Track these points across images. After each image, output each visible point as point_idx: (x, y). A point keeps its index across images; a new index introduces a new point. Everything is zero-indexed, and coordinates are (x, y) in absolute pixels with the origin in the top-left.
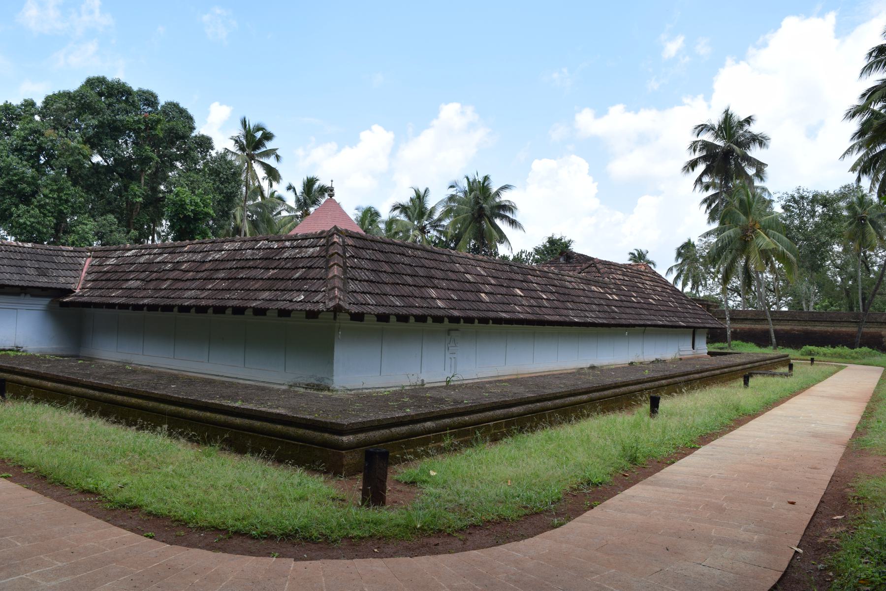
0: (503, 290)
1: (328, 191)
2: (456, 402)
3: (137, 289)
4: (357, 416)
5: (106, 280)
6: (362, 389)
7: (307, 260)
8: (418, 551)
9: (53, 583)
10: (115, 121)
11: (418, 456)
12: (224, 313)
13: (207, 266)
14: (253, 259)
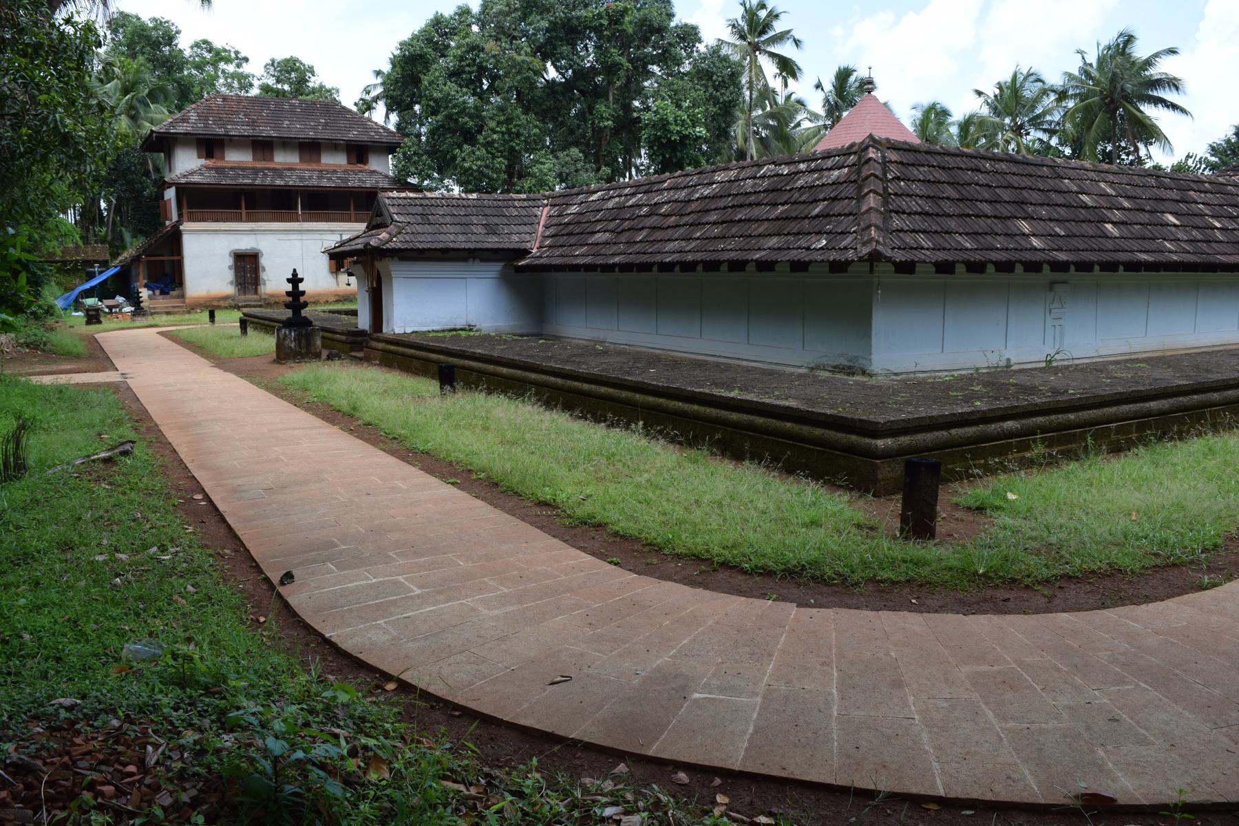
0: (1145, 217)
1: (867, 85)
2: (1055, 391)
3: (606, 243)
4: (900, 410)
5: (567, 234)
7: (830, 188)
8: (976, 606)
9: (497, 612)
10: (570, 20)
11: (989, 470)
12: (718, 270)
13: (693, 206)
14: (755, 192)
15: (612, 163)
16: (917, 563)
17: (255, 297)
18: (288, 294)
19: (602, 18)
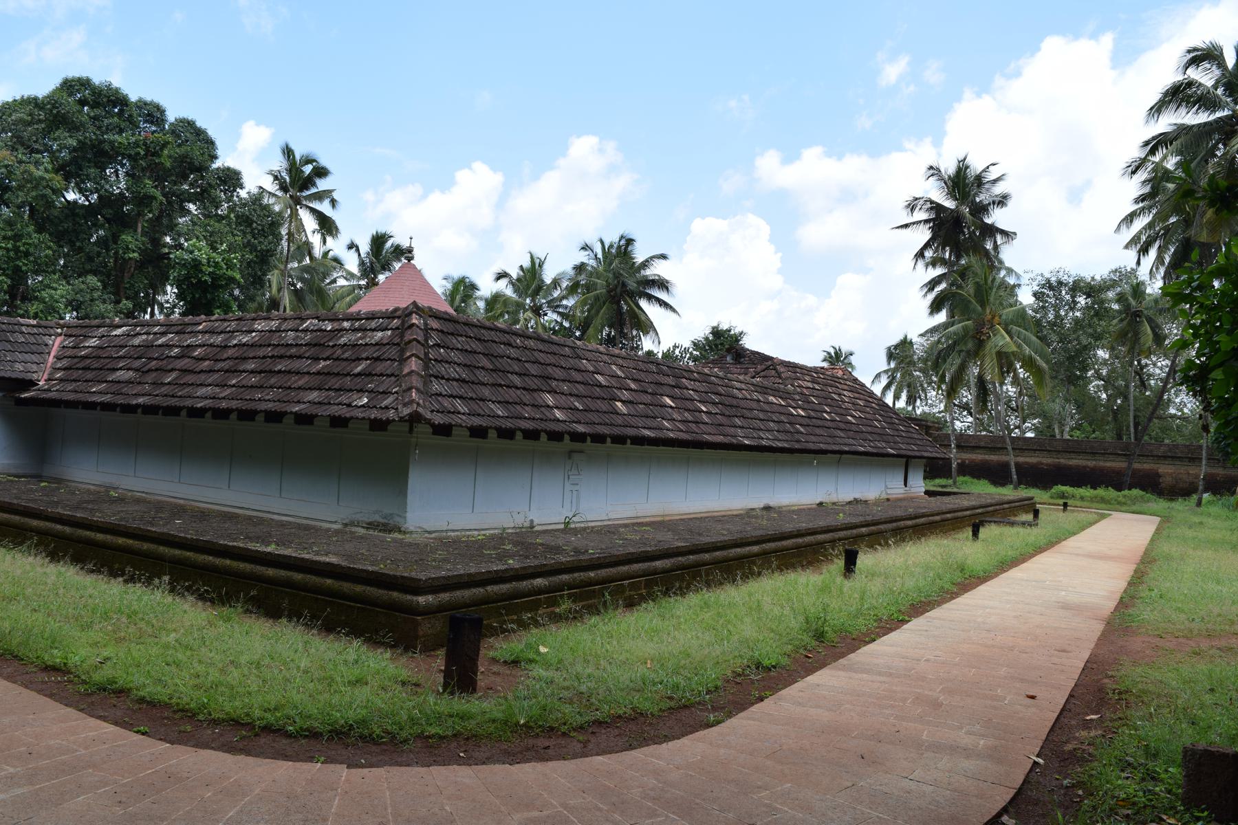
1: (403, 253)
2: (577, 551)
3: (129, 382)
4: (439, 568)
5: (83, 369)
6: (447, 531)
7: (373, 349)
8: (520, 756)
10: (102, 142)
11: (523, 625)
12: (253, 420)
13: (230, 352)
15: (134, 297)
16: (463, 717)
19: (138, 146)
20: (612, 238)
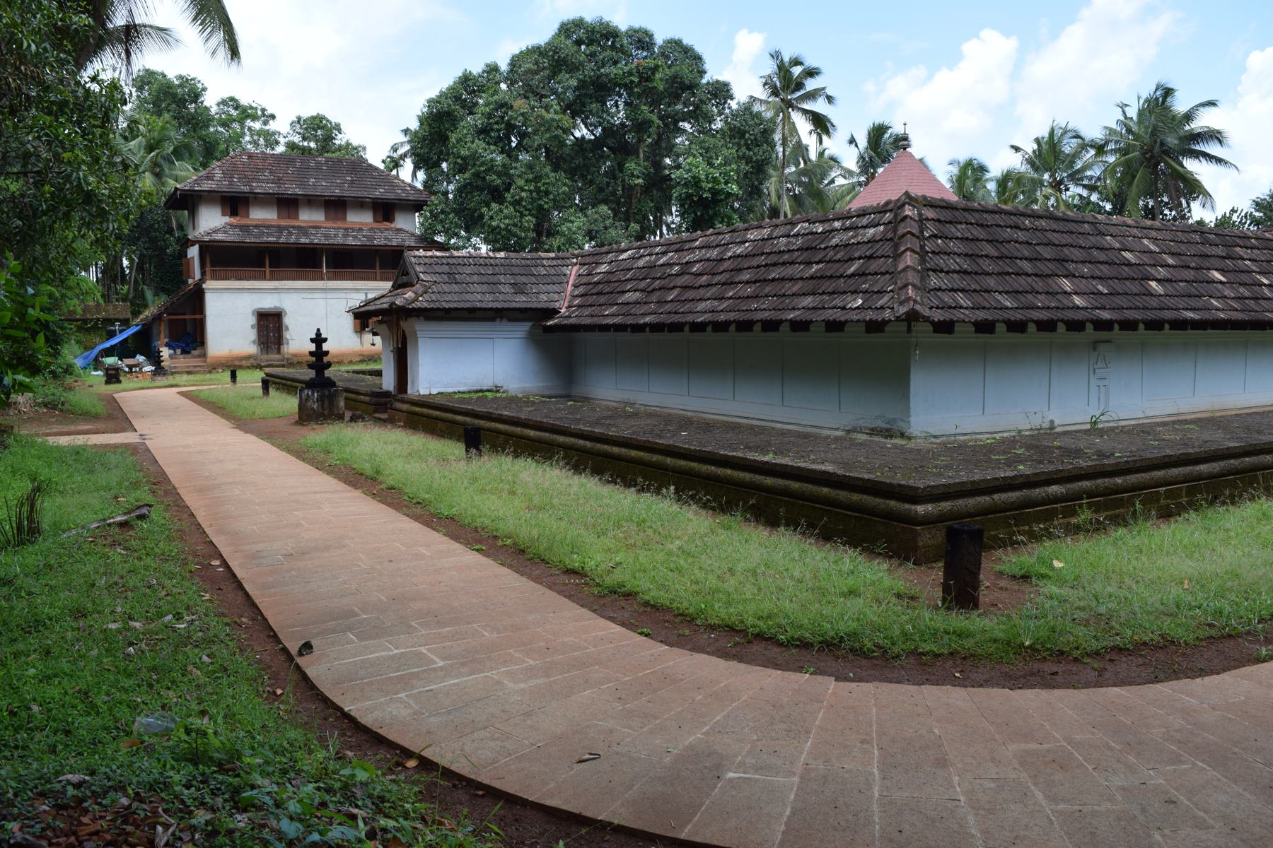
0: (1190, 274)
2: (1101, 454)
4: (940, 475)
6: (955, 435)
7: (866, 247)
8: (1023, 681)
9: (522, 685)
10: (599, 77)
11: (1034, 537)
12: (751, 330)
13: (726, 265)
16: (960, 635)
17: (278, 356)
18: (311, 354)
20: (1147, 90)
